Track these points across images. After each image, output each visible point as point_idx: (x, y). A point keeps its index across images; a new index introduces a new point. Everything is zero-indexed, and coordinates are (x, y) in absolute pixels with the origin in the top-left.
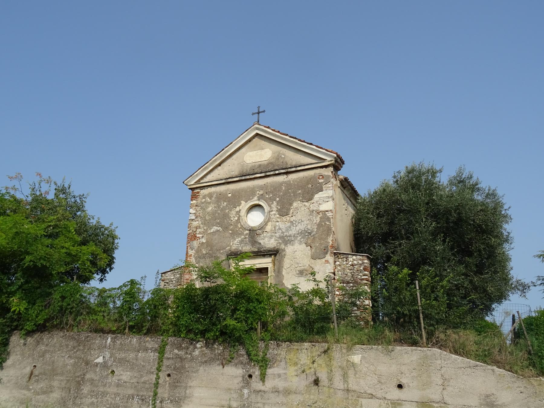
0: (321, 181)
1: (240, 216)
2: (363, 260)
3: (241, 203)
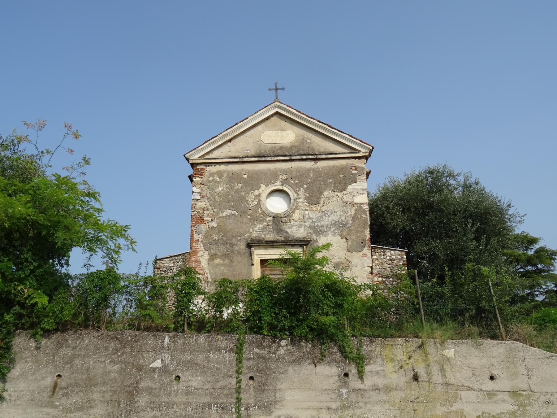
0: (354, 172)
1: (260, 201)
2: (402, 255)
3: (260, 186)
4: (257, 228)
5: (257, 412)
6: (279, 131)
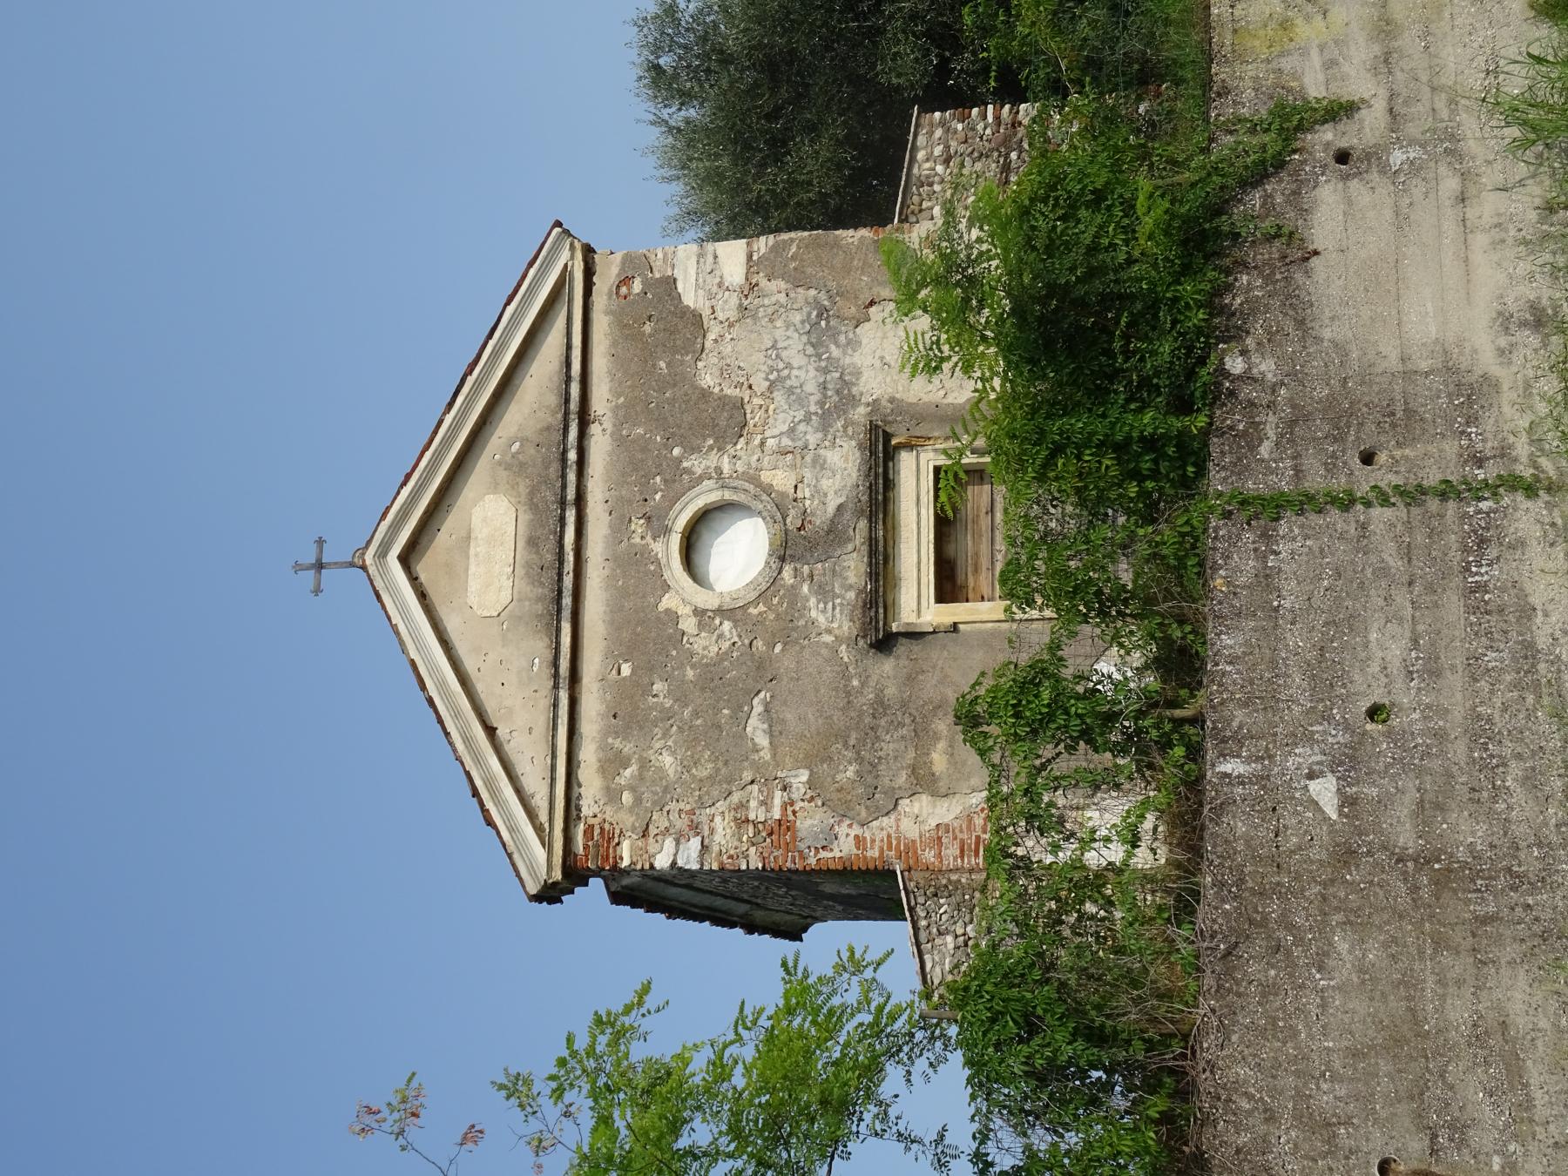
0: (637, 286)
3: (667, 611)
4: (822, 619)
5: (1489, 425)
6: (472, 551)
